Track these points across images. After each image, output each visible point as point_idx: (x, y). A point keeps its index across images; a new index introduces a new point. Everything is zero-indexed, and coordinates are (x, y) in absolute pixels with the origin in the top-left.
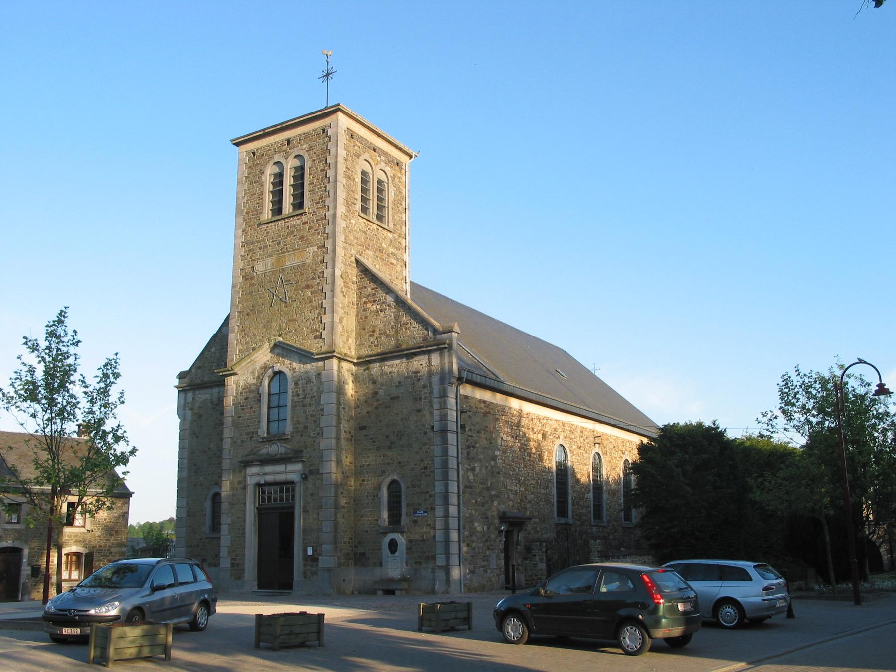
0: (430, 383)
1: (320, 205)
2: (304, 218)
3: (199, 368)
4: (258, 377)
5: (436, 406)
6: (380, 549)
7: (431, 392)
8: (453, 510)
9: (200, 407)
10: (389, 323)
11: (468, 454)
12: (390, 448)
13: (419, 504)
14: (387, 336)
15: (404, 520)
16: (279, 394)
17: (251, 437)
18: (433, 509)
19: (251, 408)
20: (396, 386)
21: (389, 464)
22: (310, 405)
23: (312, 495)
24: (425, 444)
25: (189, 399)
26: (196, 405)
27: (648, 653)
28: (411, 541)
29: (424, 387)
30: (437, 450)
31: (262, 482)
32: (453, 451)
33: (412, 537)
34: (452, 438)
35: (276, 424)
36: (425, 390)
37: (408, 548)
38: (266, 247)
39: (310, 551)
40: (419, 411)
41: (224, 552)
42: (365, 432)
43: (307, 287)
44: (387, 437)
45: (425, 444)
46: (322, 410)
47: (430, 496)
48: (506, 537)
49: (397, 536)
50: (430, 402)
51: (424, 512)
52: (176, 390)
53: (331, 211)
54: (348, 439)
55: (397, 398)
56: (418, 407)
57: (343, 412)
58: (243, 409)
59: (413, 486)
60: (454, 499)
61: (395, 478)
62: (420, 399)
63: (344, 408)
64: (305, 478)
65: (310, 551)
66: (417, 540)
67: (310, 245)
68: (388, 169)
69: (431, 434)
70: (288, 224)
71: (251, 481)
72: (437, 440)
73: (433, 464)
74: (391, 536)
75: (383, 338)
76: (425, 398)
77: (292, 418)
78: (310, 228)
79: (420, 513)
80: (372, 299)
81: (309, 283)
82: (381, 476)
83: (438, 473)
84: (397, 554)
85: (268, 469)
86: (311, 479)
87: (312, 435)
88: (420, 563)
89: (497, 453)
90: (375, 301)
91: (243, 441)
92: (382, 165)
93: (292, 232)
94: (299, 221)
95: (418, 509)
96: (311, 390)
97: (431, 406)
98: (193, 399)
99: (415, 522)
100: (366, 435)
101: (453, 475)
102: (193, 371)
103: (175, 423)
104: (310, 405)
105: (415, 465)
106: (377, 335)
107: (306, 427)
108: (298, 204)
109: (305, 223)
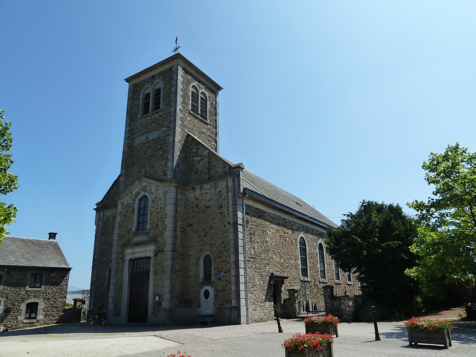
0: (228, 197)
1: (168, 106)
2: (160, 114)
3: (107, 199)
4: (134, 199)
5: (231, 210)
6: (199, 296)
7: (228, 202)
8: (242, 272)
9: (106, 220)
10: (205, 166)
11: (251, 238)
12: (205, 236)
13: (222, 268)
14: (204, 173)
15: (213, 278)
16: (144, 208)
17: (129, 233)
18: (230, 271)
19: (129, 216)
20: (209, 200)
21: (204, 245)
22: (160, 212)
23: (159, 264)
24: (225, 232)
25: (101, 216)
26: (105, 218)
27: (70, 265)
28: (217, 291)
29: (224, 199)
30: (231, 236)
31: (133, 258)
32: (240, 236)
33: (219, 288)
34: (240, 228)
35: (142, 225)
36: (224, 202)
37: (216, 296)
38: (140, 131)
39: (157, 299)
40: (221, 213)
41: (111, 300)
42: (191, 228)
43: (161, 149)
44: (204, 229)
45: (225, 232)
46: (166, 215)
47: (228, 263)
48: (274, 288)
49: (209, 288)
50: (228, 208)
51: (225, 273)
52: (95, 212)
53: (173, 109)
54: (182, 232)
55: (209, 207)
56: (221, 211)
57: (179, 216)
58: (125, 217)
59: (218, 258)
60: (241, 264)
61: (208, 253)
62: (222, 206)
63: (180, 214)
64: (156, 253)
65: (157, 299)
66: (220, 290)
67: (163, 126)
68: (206, 93)
69: (228, 226)
70: (153, 118)
71: (128, 258)
72: (231, 230)
73: (229, 244)
74: (205, 288)
75: (202, 174)
76: (225, 206)
77: (150, 220)
78: (163, 119)
79: (222, 274)
80: (196, 154)
81: (162, 146)
82: (200, 252)
83: (232, 250)
84: (209, 299)
85: (137, 250)
86: (159, 254)
87: (161, 229)
88: (223, 305)
89: (267, 239)
90: (198, 155)
91: (124, 235)
92: (203, 90)
93: (154, 122)
94: (157, 116)
95: (221, 271)
96: (161, 203)
97: (228, 210)
98: (103, 215)
99: (219, 279)
100: (192, 229)
101: (241, 250)
102: (104, 200)
103: (93, 228)
104: (160, 212)
105: (220, 245)
106: (199, 173)
107: (157, 225)
108: (157, 107)
109: (160, 116)
